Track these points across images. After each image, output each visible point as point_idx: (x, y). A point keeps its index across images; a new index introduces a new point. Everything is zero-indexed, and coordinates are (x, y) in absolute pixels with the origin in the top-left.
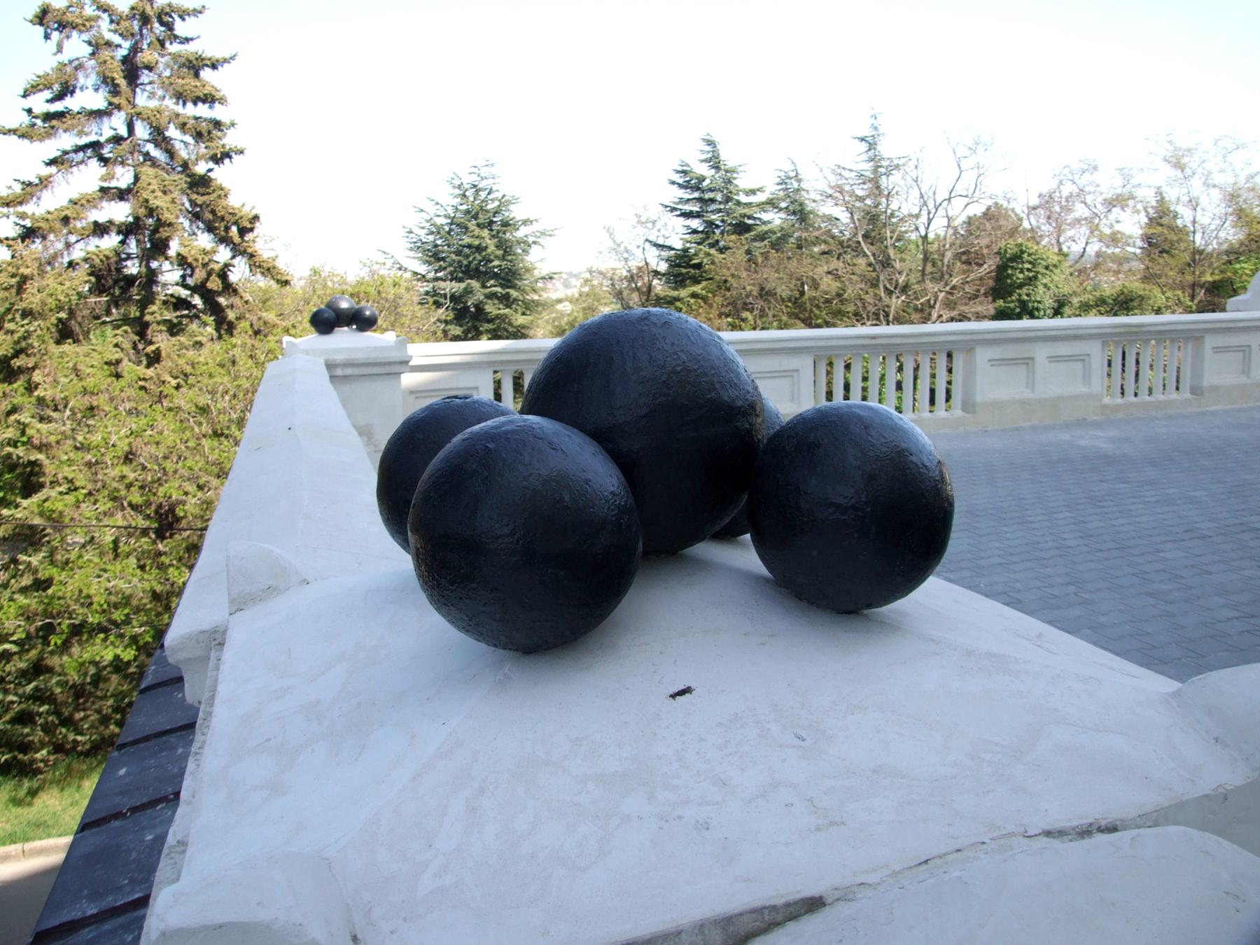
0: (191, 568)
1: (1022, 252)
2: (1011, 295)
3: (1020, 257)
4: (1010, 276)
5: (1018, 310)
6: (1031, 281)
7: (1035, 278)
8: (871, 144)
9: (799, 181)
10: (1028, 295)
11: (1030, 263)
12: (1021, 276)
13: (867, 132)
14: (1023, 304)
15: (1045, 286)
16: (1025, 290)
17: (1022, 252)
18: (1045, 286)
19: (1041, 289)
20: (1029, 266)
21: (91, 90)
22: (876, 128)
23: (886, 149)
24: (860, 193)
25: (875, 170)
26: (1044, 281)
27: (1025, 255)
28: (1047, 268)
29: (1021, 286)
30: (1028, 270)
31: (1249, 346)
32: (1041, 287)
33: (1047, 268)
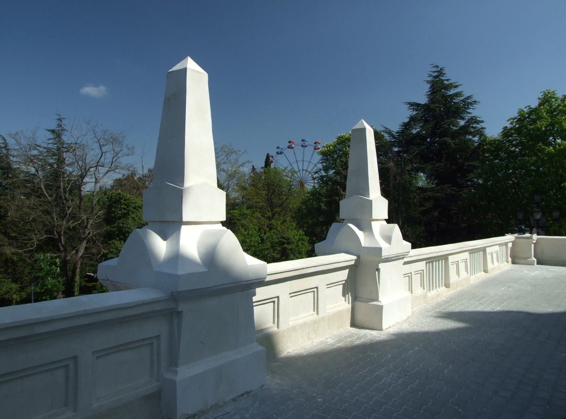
0: (125, 241)
1: (121, 199)
2: (115, 223)
3: (119, 201)
4: (114, 212)
5: (117, 232)
6: (126, 215)
7: (128, 214)
8: (57, 134)
9: (8, 150)
10: (123, 224)
11: (125, 205)
12: (120, 212)
13: (54, 126)
14: (120, 229)
15: (133, 218)
16: (121, 221)
17: (121, 199)
18: (133, 218)
19: (130, 220)
20: (125, 207)
21: (273, 153)
22: (61, 126)
23: (66, 138)
24: (52, 161)
25: (59, 149)
26: (133, 216)
27: (122, 201)
28: (135, 208)
29: (120, 218)
30: (124, 209)
31: (75, 358)
32: (131, 219)
33: (135, 208)
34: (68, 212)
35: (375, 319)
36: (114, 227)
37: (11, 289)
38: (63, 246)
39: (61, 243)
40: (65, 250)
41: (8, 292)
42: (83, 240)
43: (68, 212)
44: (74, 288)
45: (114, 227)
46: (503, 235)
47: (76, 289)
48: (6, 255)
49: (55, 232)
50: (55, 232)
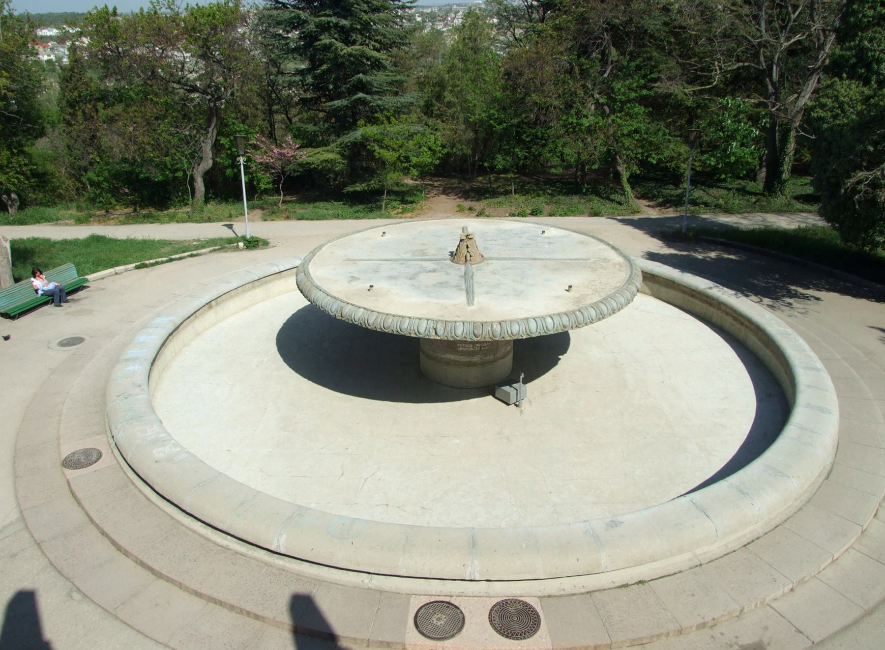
5: (854, 60)
10: (871, 41)
12: (871, 13)
14: (861, 52)
16: (870, 34)
34: (793, 17)
35: (283, 623)
36: (850, 49)
37: (680, 154)
38: (773, 84)
39: (771, 80)
40: (776, 94)
41: (672, 159)
42: (812, 74)
43: (793, 17)
44: (782, 165)
45: (850, 49)
46: (640, 219)
47: (785, 167)
48: (676, 96)
49: (762, 58)
50: (762, 58)
